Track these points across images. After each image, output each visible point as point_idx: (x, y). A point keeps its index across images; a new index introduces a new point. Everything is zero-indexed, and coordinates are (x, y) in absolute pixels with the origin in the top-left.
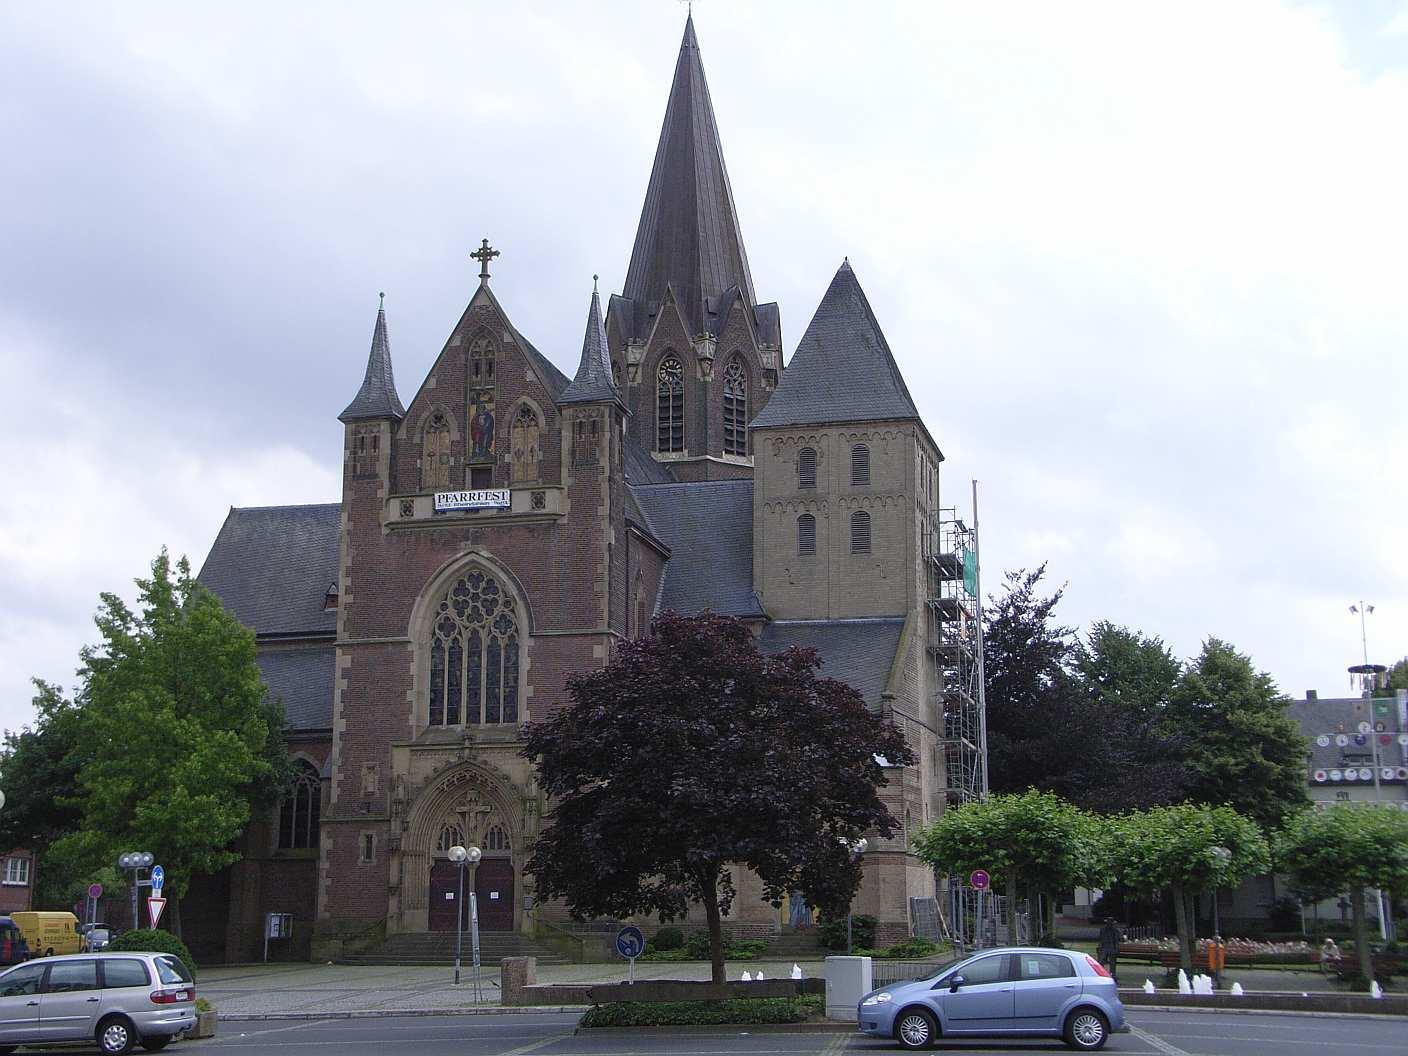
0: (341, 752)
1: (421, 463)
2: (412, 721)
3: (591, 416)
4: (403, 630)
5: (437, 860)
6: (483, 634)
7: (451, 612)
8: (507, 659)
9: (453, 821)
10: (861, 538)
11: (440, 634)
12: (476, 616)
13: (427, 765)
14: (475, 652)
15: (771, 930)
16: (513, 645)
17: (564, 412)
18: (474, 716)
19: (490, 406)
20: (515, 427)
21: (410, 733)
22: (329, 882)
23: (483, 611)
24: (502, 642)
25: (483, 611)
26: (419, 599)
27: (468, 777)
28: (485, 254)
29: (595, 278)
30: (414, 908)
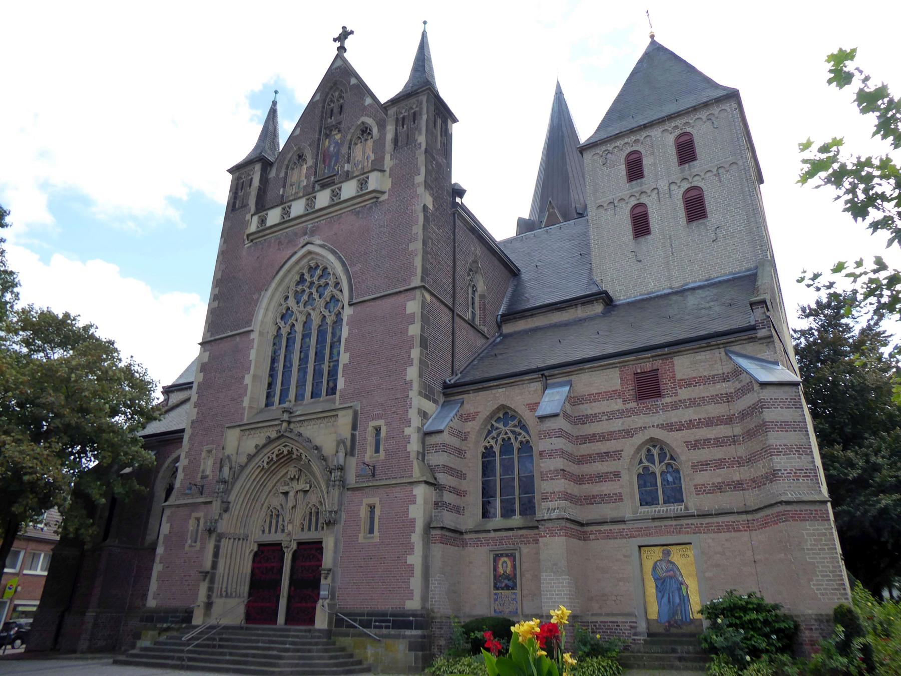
1: (284, 191)
2: (246, 403)
3: (412, 108)
4: (249, 322)
5: (260, 545)
7: (291, 302)
8: (334, 334)
9: (276, 501)
10: (695, 208)
11: (282, 324)
13: (251, 443)
15: (631, 627)
18: (299, 397)
21: (243, 414)
23: (316, 295)
24: (329, 320)
25: (316, 295)
28: (345, 34)
30: (227, 596)
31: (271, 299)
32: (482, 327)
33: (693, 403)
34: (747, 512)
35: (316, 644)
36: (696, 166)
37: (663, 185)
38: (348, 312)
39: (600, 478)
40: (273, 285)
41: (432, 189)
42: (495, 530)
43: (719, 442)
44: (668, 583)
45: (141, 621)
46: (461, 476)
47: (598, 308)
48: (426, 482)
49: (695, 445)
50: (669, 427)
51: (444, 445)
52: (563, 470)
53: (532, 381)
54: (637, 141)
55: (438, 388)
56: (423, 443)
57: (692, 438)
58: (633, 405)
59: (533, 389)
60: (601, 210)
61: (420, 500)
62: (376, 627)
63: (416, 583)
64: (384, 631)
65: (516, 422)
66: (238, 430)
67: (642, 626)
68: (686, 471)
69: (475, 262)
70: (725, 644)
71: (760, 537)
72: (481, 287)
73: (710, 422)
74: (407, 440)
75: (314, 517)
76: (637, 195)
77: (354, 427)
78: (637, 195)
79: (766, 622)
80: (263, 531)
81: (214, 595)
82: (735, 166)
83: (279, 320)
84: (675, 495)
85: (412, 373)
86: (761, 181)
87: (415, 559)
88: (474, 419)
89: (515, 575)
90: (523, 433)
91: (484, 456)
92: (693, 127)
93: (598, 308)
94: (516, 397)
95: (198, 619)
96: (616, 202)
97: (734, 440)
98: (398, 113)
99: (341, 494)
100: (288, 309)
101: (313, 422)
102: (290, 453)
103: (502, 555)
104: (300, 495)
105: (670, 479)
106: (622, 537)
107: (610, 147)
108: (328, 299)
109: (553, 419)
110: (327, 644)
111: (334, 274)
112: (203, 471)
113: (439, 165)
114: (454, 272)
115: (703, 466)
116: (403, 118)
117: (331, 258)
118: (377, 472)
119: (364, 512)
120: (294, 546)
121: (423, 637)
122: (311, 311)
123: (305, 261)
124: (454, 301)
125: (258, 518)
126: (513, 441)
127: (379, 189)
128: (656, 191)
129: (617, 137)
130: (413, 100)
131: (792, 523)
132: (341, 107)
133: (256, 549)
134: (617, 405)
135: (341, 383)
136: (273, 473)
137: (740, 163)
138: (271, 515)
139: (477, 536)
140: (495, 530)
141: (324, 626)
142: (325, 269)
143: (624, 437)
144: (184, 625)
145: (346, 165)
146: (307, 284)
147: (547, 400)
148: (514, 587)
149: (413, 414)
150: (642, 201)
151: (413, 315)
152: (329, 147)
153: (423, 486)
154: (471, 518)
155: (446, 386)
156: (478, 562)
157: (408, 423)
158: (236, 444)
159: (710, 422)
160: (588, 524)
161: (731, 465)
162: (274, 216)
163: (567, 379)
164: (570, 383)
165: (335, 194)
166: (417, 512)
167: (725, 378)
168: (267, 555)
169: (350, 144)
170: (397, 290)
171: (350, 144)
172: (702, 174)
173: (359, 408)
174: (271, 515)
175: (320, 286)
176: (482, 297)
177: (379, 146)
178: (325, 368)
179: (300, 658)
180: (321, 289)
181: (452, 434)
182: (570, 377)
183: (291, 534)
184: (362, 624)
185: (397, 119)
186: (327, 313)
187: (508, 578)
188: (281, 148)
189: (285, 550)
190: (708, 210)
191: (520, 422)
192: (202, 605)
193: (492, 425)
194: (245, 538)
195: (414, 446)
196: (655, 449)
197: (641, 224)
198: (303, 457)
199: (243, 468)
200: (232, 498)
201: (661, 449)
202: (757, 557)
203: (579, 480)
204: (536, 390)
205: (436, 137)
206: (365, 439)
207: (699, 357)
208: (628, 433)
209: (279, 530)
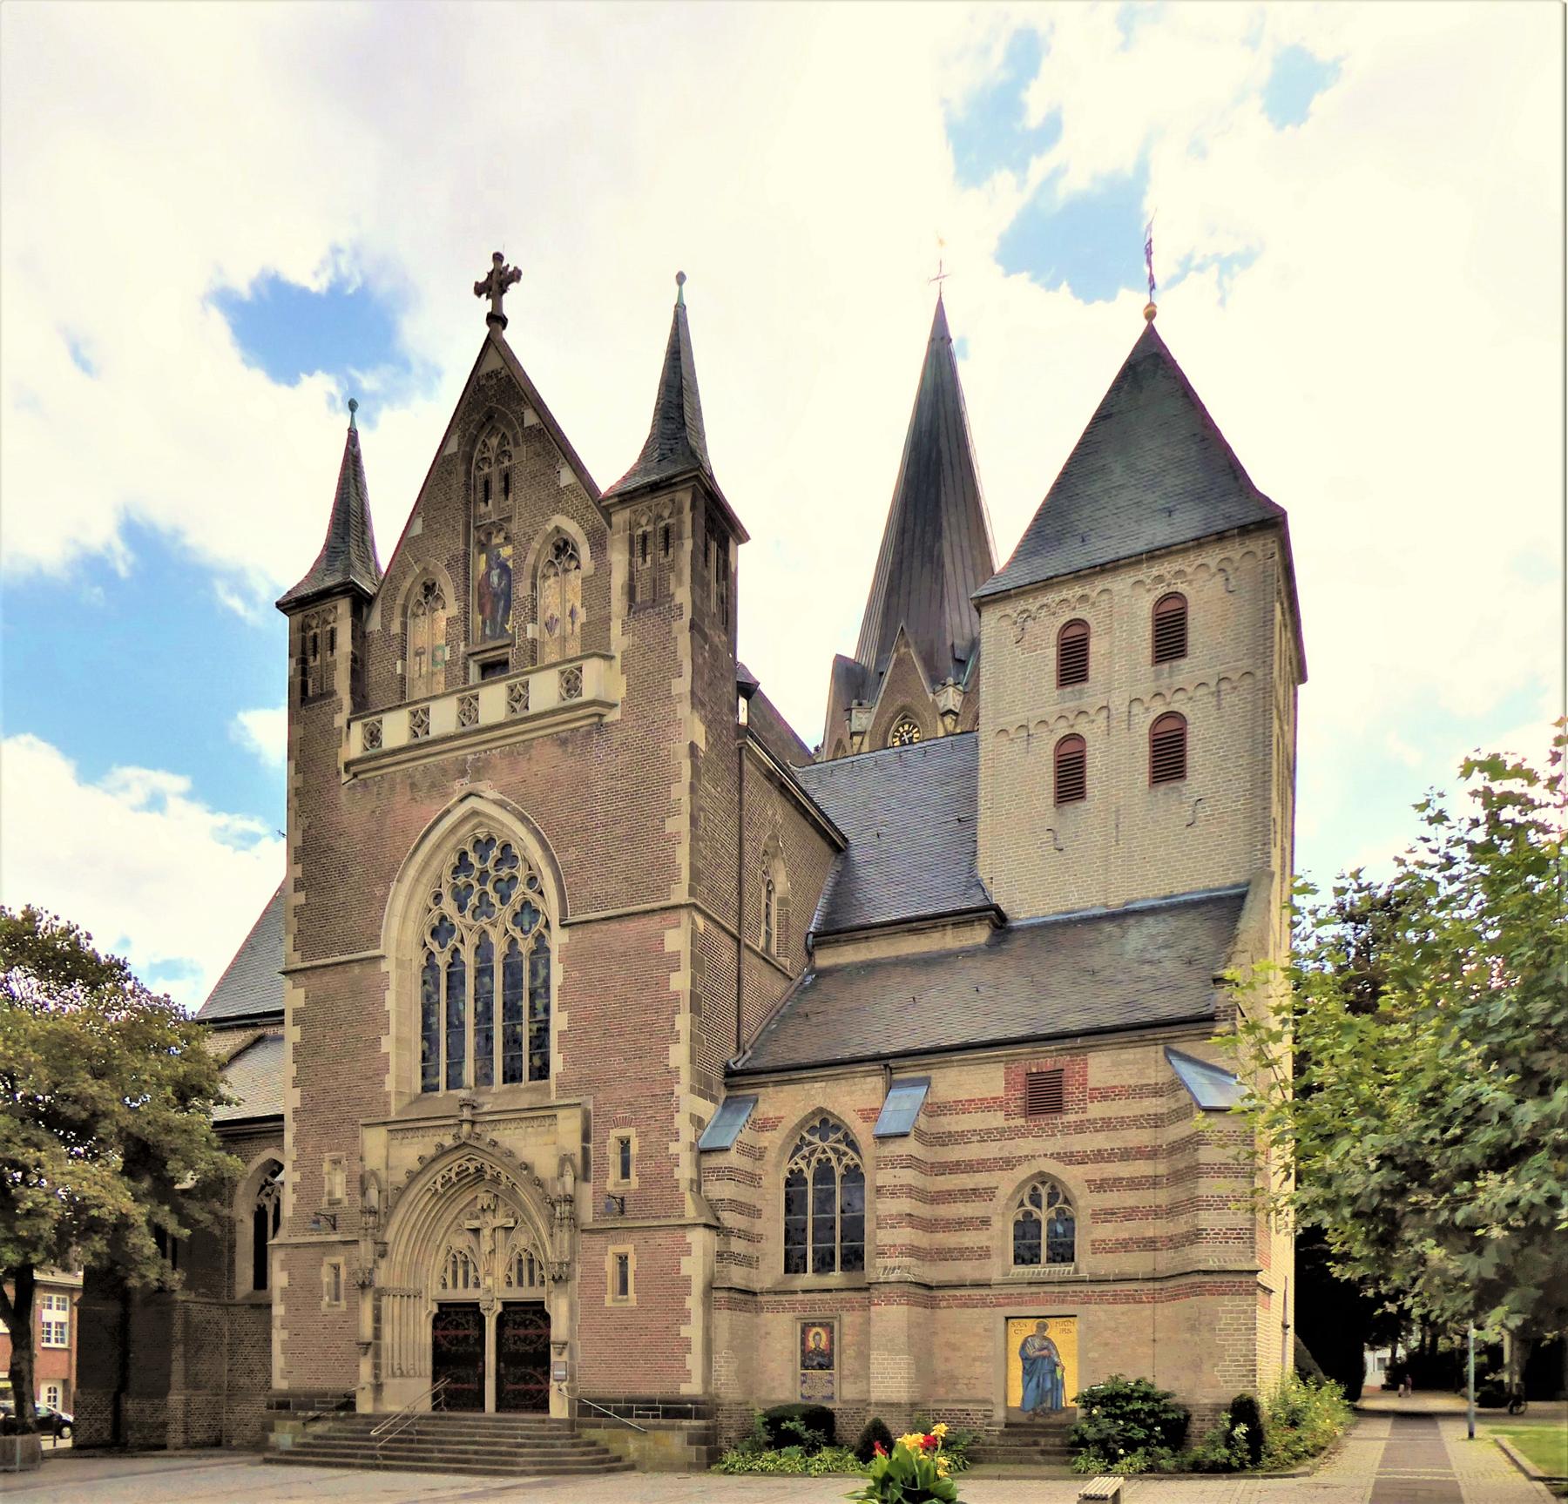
0: (297, 1140)
1: (404, 667)
2: (390, 1084)
3: (660, 517)
4: (374, 940)
6: (495, 936)
7: (448, 906)
8: (534, 974)
9: (461, 1242)
11: (434, 946)
12: (484, 908)
13: (411, 1152)
14: (484, 971)
16: (541, 950)
17: (614, 519)
18: (484, 1078)
19: (506, 552)
20: (545, 577)
21: (387, 1103)
22: (284, 1335)
23: (494, 898)
24: (526, 946)
25: (494, 898)
26: (394, 885)
27: (472, 1170)
28: (497, 282)
29: (681, 278)
30: (402, 1375)
31: (410, 898)
32: (781, 959)
33: (1107, 1124)
34: (1154, 1279)
35: (558, 1438)
36: (1185, 670)
37: (1119, 703)
38: (558, 939)
39: (962, 1224)
40: (412, 872)
41: (703, 705)
42: (805, 1292)
43: (1134, 1184)
44: (1040, 1366)
45: (269, 1407)
46: (752, 1212)
47: (980, 935)
48: (706, 1226)
49: (1101, 1186)
50: (1068, 1158)
51: (731, 1170)
52: (910, 1215)
53: (868, 1074)
54: (1084, 598)
55: (717, 1076)
56: (698, 1165)
57: (1097, 1177)
58: (1021, 1122)
59: (870, 1086)
60: (1003, 738)
61: (697, 1250)
62: (638, 1416)
63: (694, 1361)
64: (651, 1421)
65: (840, 1135)
66: (383, 1131)
67: (999, 1415)
68: (1082, 1222)
69: (774, 837)
70: (1097, 1437)
71: (1166, 1310)
72: (782, 884)
73: (1126, 1155)
74: (675, 1161)
75: (526, 1267)
76: (1071, 717)
77: (586, 1137)
78: (1071, 717)
79: (1151, 1413)
80: (445, 1285)
81: (383, 1374)
82: (1249, 680)
83: (428, 939)
84: (1063, 1252)
85: (679, 1055)
86: (1302, 677)
87: (693, 1331)
88: (774, 1128)
89: (832, 1350)
90: (851, 1153)
91: (788, 1183)
92: (1190, 582)
93: (980, 935)
94: (848, 1098)
95: (364, 1406)
96: (1031, 725)
97: (1154, 1182)
98: (632, 525)
99: (572, 1237)
100: (443, 918)
101: (514, 1125)
102: (480, 1170)
103: (814, 1325)
104: (500, 1234)
105: (1060, 1229)
106: (985, 1305)
107: (1031, 604)
108: (518, 908)
109: (899, 1141)
110: (573, 1437)
111: (525, 860)
112: (330, 1193)
113: (714, 651)
114: (741, 866)
115: (1108, 1215)
116: (644, 537)
117: (520, 829)
118: (627, 1208)
119: (610, 1265)
120: (499, 1308)
121: (707, 1428)
122: (488, 927)
123: (468, 827)
124: (740, 920)
125: (436, 1264)
126: (834, 1163)
127: (603, 698)
128: (1104, 713)
129: (1049, 583)
130: (663, 498)
131: (1208, 1297)
132: (507, 478)
133: (436, 1310)
134: (997, 1120)
135: (557, 1063)
136: (452, 1200)
137: (1259, 674)
138: (455, 1263)
139: (777, 1298)
140: (805, 1292)
141: (565, 1415)
142: (506, 847)
143: (1001, 1169)
144: (342, 1414)
145: (530, 626)
146: (476, 874)
147: (891, 1108)
148: (829, 1366)
149: (682, 1122)
150: (1077, 730)
151: (676, 955)
152: (488, 574)
153: (701, 1232)
154: (771, 1269)
155: (729, 1073)
156: (779, 1334)
157: (676, 1136)
158: (383, 1152)
159: (1126, 1155)
160: (939, 1287)
161: (1146, 1216)
162: (396, 729)
163: (922, 1074)
164: (927, 1082)
165: (518, 698)
166: (695, 1267)
167: (1157, 1092)
168: (455, 1320)
169: (534, 577)
170: (647, 906)
171: (534, 577)
172: (1190, 688)
173: (591, 1107)
174: (455, 1263)
175: (500, 880)
176: (783, 902)
177: (596, 588)
178: (526, 1031)
179: (544, 1454)
180: (501, 885)
181: (742, 1152)
182: (929, 1073)
183: (493, 1289)
184: (617, 1411)
185: (631, 537)
186: (518, 934)
187: (821, 1354)
188: (384, 569)
189: (486, 1313)
190: (1190, 762)
191: (846, 1135)
192: (368, 1387)
193: (802, 1138)
194: (418, 1295)
195: (685, 1172)
196: (1046, 1189)
197: (1070, 779)
198: (504, 1179)
199: (401, 1191)
200: (389, 1236)
201: (1053, 1187)
202: (1158, 1336)
203: (930, 1226)
204: (874, 1089)
205: (708, 585)
206: (605, 1157)
207: (1124, 1056)
208: (1008, 1163)
209: (471, 1284)
